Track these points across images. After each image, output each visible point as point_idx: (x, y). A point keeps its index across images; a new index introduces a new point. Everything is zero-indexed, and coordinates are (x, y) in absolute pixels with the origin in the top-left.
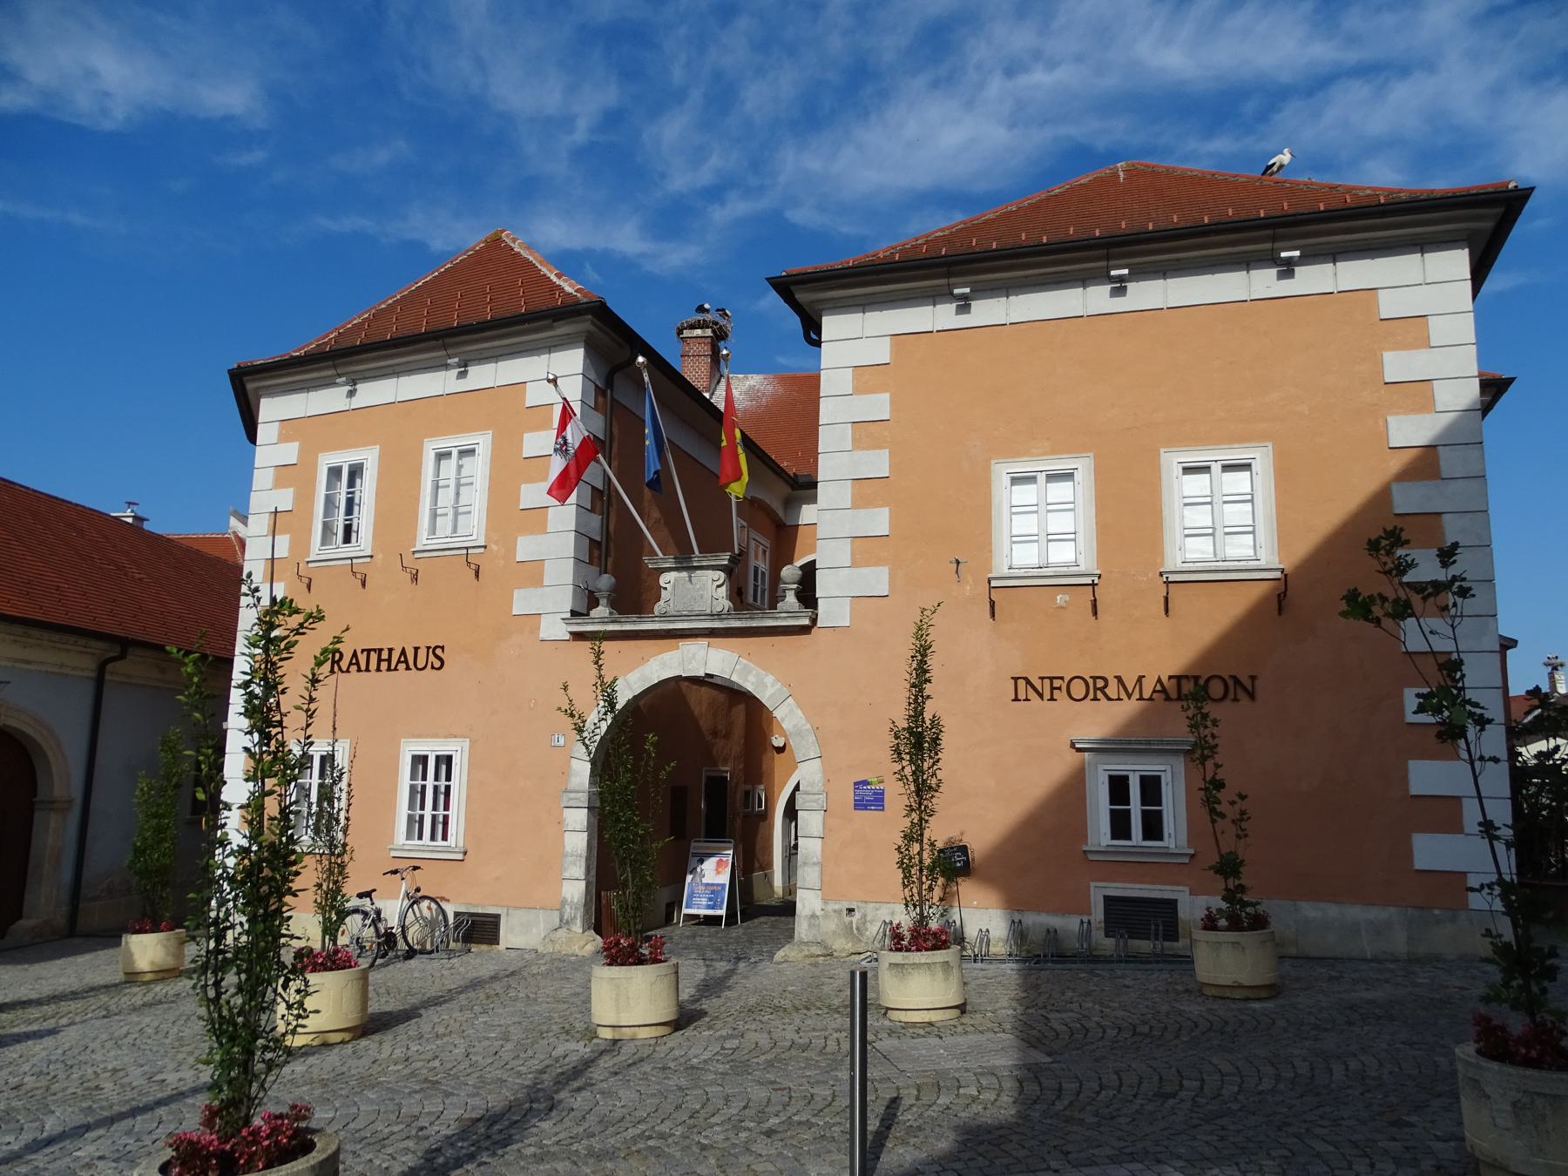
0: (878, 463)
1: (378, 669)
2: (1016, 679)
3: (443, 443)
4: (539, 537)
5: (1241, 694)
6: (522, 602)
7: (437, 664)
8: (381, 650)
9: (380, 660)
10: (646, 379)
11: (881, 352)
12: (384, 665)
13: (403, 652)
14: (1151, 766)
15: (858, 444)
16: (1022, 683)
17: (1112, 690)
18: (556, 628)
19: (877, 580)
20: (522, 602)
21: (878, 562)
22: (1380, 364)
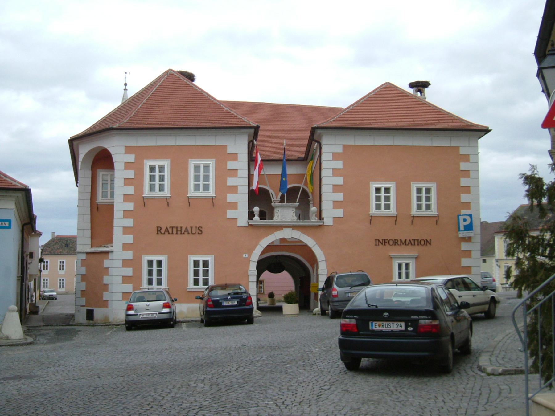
0: (339, 181)
1: (177, 233)
2: (376, 240)
3: (197, 162)
4: (466, 179)
5: (428, 244)
6: (231, 214)
7: (200, 232)
8: (177, 227)
9: (177, 230)
10: (415, 317)
11: (340, 150)
12: (179, 232)
13: (186, 228)
14: (407, 261)
15: (124, 282)
16: (377, 241)
17: (399, 243)
18: (243, 221)
19: (339, 213)
20: (231, 214)
21: (340, 208)
22: (459, 165)
